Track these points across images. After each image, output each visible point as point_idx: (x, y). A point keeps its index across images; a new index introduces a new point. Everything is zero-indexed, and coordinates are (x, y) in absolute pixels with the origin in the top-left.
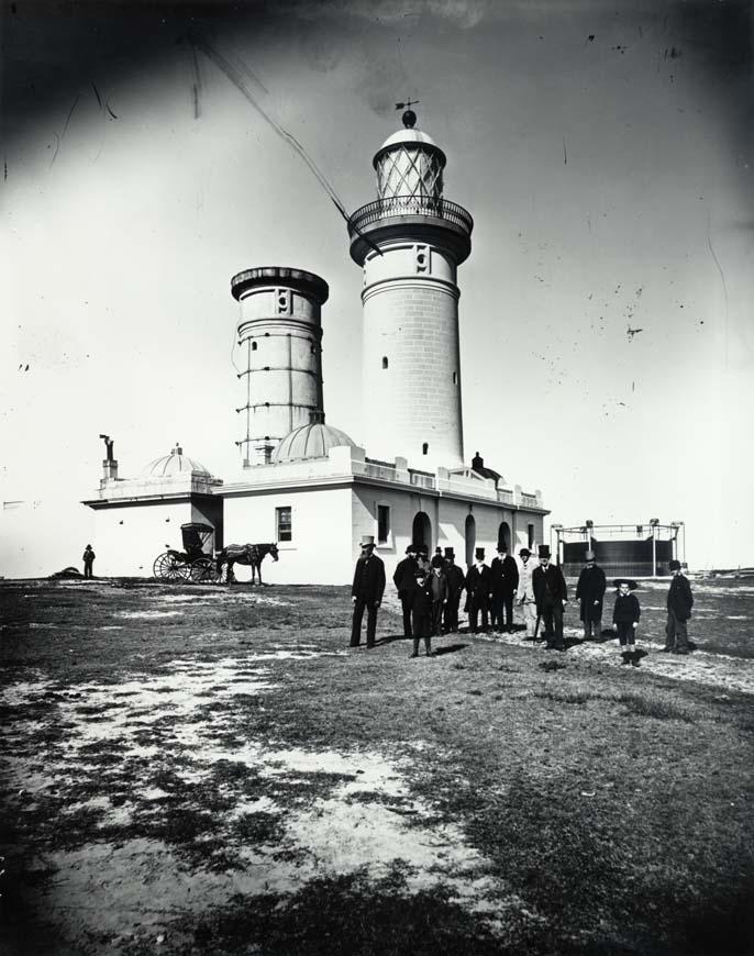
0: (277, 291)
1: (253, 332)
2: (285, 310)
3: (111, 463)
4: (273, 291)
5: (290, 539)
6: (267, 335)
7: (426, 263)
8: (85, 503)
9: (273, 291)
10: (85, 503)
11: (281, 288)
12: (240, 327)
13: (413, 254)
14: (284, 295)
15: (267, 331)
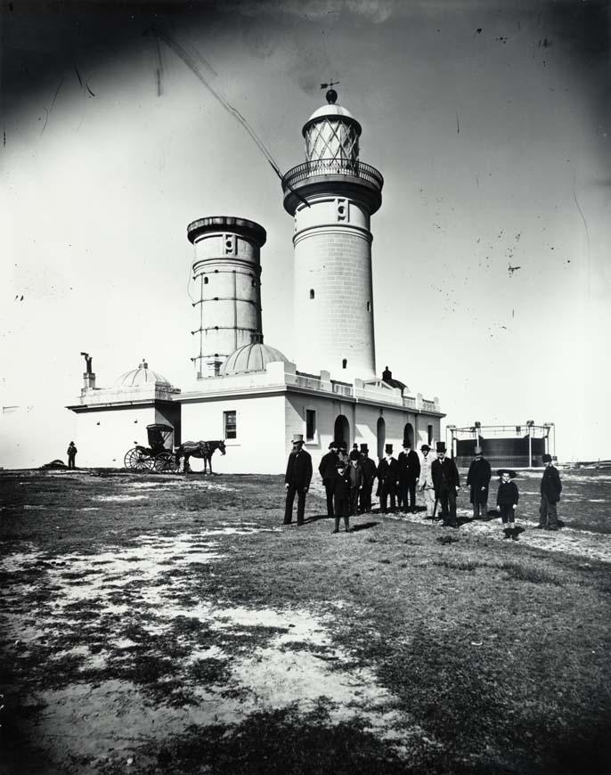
0: (224, 236)
1: (205, 269)
2: (231, 251)
3: (90, 375)
4: (221, 236)
5: (235, 437)
6: (216, 271)
7: (345, 213)
8: (69, 408)
9: (221, 236)
10: (69, 408)
11: (228, 233)
12: (195, 265)
13: (335, 206)
14: (230, 239)
15: (216, 268)
